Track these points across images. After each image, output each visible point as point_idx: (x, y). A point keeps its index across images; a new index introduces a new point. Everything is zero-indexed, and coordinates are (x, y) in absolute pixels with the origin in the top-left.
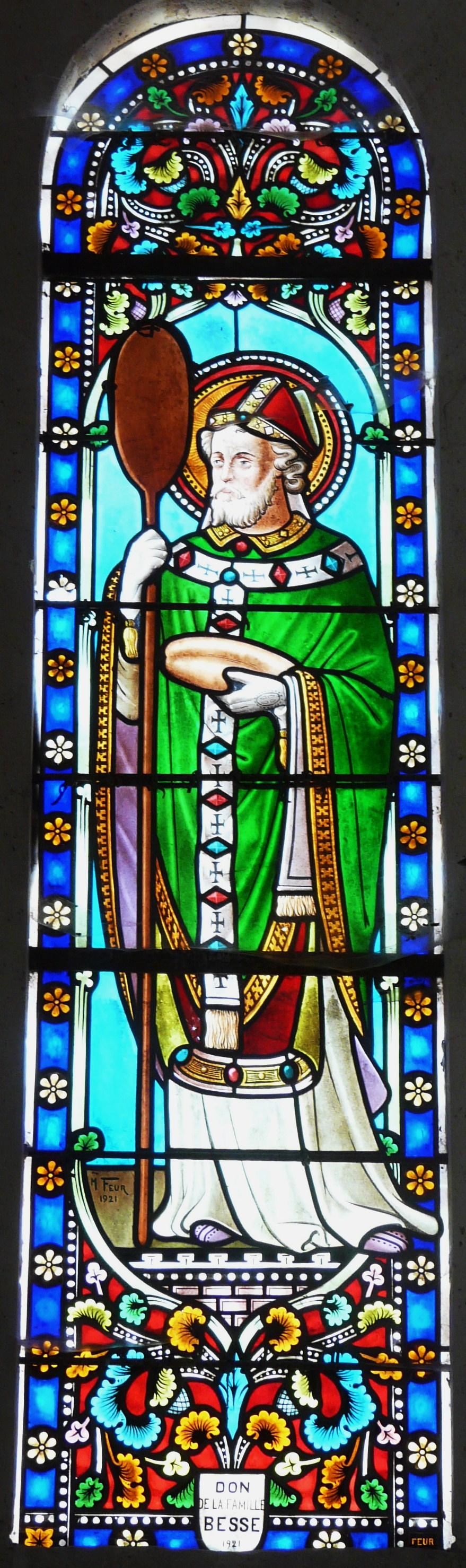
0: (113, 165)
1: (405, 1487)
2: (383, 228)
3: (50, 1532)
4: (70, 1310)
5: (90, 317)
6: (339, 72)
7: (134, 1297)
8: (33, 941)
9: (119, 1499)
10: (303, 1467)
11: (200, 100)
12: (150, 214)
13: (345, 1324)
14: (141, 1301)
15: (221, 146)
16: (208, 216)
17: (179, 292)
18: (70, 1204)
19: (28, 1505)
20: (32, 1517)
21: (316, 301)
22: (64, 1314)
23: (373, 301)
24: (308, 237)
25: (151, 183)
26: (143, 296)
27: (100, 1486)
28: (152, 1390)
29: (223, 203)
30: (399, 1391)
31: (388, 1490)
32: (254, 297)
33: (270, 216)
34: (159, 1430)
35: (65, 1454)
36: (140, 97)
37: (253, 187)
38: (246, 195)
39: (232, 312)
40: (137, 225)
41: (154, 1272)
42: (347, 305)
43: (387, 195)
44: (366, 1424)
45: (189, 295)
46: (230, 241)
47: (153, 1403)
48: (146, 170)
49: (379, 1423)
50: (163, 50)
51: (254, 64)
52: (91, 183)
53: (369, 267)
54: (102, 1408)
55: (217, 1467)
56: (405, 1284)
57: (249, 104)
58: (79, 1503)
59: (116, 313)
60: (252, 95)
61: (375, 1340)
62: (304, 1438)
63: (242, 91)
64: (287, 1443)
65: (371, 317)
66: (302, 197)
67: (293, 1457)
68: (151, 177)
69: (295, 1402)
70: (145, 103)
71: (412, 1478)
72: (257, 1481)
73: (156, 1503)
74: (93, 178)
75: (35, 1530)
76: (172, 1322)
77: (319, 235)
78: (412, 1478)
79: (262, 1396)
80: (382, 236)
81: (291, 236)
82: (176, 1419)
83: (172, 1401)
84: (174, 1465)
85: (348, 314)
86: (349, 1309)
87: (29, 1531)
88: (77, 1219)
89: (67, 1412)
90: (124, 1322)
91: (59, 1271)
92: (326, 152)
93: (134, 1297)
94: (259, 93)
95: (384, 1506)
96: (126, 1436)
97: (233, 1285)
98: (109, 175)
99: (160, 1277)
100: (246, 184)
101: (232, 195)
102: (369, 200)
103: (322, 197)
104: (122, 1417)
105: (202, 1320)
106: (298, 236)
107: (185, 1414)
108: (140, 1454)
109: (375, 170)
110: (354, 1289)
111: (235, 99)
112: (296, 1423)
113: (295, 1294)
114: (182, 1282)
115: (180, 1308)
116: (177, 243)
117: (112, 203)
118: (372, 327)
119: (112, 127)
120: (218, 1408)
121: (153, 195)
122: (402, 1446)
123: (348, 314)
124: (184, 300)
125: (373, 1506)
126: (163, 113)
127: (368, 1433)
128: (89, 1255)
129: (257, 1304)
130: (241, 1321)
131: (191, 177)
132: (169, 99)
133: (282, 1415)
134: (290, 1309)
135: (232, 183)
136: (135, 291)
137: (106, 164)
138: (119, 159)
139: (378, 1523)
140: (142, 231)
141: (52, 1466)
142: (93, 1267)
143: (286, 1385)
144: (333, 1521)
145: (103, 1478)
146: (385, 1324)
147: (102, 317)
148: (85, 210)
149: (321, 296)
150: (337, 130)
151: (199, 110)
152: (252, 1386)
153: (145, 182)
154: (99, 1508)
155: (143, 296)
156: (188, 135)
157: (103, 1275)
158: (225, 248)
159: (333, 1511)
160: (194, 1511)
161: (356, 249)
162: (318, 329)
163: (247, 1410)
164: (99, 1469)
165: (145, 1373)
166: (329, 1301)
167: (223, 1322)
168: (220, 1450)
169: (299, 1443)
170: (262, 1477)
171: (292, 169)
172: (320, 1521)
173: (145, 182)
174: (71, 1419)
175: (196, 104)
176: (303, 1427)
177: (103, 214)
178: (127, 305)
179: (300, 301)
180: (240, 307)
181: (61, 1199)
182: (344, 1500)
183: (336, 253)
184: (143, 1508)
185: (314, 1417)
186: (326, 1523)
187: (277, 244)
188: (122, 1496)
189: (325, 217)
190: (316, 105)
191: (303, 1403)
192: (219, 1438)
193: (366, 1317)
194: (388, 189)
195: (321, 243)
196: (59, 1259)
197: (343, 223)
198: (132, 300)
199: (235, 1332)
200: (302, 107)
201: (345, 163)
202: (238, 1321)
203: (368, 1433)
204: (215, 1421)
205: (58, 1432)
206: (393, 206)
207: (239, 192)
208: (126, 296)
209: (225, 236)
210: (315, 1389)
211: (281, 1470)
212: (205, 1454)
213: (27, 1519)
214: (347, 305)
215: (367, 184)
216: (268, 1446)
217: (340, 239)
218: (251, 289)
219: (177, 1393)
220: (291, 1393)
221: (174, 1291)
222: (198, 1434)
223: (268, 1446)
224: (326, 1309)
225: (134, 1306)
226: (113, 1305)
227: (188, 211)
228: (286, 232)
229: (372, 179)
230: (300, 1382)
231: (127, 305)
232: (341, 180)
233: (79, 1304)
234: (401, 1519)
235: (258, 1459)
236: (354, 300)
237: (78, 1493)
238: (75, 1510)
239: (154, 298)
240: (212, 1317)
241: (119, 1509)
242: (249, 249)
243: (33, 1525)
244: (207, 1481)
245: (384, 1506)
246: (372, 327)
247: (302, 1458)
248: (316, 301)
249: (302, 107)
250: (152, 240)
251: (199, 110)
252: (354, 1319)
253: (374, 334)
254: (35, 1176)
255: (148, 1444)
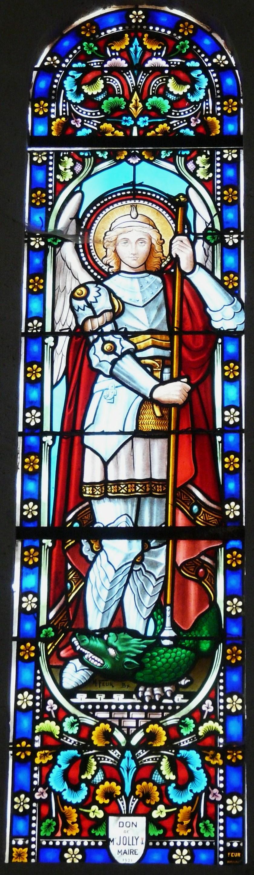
0: (65, 86)
1: (224, 824)
2: (218, 118)
3: (26, 850)
4: (37, 727)
5: (51, 172)
6: (191, 32)
7: (72, 718)
8: (18, 523)
9: (65, 830)
10: (166, 813)
11: (113, 48)
12: (85, 112)
13: (191, 734)
14: (76, 720)
15: (124, 74)
16: (118, 114)
17: (100, 155)
18: (38, 666)
19: (14, 833)
20: (16, 842)
21: (180, 161)
22: (34, 729)
23: (211, 160)
24: (175, 125)
25: (86, 95)
26: (81, 160)
27: (54, 823)
28: (84, 769)
29: (127, 106)
30: (221, 771)
31: (215, 827)
32: (146, 157)
33: (153, 114)
34: (86, 793)
35: (34, 805)
36: (79, 48)
37: (144, 98)
38: (139, 102)
39: (132, 167)
40: (80, 120)
41: (86, 704)
42: (197, 162)
43: (218, 100)
44: (203, 788)
45: (106, 157)
46: (131, 127)
47: (83, 777)
48: (84, 87)
49: (210, 788)
50: (91, 21)
51: (142, 27)
52: (53, 97)
53: (204, 140)
54: (56, 781)
55: (119, 812)
56: (225, 710)
57: (140, 49)
58: (42, 834)
59: (65, 169)
60: (141, 44)
61: (209, 741)
62: (168, 795)
63: (136, 42)
64: (158, 799)
65: (211, 170)
66: (171, 103)
67: (161, 807)
68: (86, 91)
69: (163, 777)
70: (83, 52)
71: (228, 819)
72: (141, 821)
73: (85, 834)
74: (54, 95)
75: (18, 849)
76: (94, 733)
77: (180, 124)
78: (228, 819)
79: (144, 773)
80: (218, 122)
81: (165, 125)
82: (97, 786)
83: (93, 776)
84: (96, 813)
85: (198, 167)
86: (194, 726)
87: (14, 849)
88: (41, 675)
89: (35, 783)
90: (67, 733)
91: (30, 704)
92: (182, 75)
93: (72, 718)
94: (145, 43)
95: (213, 835)
96: (67, 796)
97: (129, 712)
98: (63, 91)
99: (82, 707)
100: (140, 95)
101: (132, 102)
102: (208, 102)
103: (179, 103)
104: (66, 786)
105: (110, 730)
106: (169, 125)
107: (103, 782)
108: (76, 806)
109: (210, 85)
110: (62, 714)
111: (132, 46)
112: (163, 788)
113: (163, 718)
114: (102, 710)
115: (98, 725)
116: (101, 129)
117: (65, 108)
118: (211, 175)
119: (64, 65)
120: (120, 781)
121: (90, 102)
122: (223, 802)
123: (198, 167)
124: (103, 160)
125: (206, 835)
126: (93, 56)
127: (204, 794)
128: (47, 695)
129: (142, 723)
130: (133, 731)
131: (109, 90)
132: (96, 48)
133: (155, 783)
134: (160, 725)
135: (132, 95)
136: (76, 157)
137: (61, 86)
138: (68, 83)
139: (208, 844)
140: (82, 123)
141: (27, 814)
142: (50, 702)
143: (157, 766)
144: (182, 843)
145: (56, 819)
146: (213, 734)
147: (58, 171)
148: (49, 113)
149: (183, 158)
150: (188, 64)
151: (114, 54)
152: (139, 767)
153: (82, 95)
154: (53, 836)
155: (81, 160)
156: (107, 69)
157: (55, 707)
158: (128, 133)
159: (183, 837)
160: (107, 840)
161: (201, 130)
162: (180, 175)
163: (136, 781)
164: (54, 815)
165: (81, 764)
166: (183, 721)
167: (122, 732)
168: (120, 803)
169: (165, 800)
170: (144, 819)
171: (165, 87)
172: (175, 843)
173: (82, 95)
174: (37, 787)
175: (112, 51)
176: (167, 790)
177: (61, 114)
178: (72, 164)
179: (171, 160)
180: (137, 164)
181: (32, 665)
182: (189, 831)
183: (192, 133)
184: (78, 836)
185: (173, 785)
186: (72, 844)
187: (157, 130)
188: (67, 828)
189: (185, 113)
190: (178, 49)
191: (167, 778)
192: (119, 797)
193: (202, 731)
194: (219, 96)
195: (184, 128)
196: (31, 697)
197: (195, 115)
198: (75, 161)
199: (129, 737)
200: (169, 51)
201: (194, 81)
202: (132, 730)
203: (204, 794)
204: (119, 788)
205: (30, 794)
206: (222, 106)
207: (136, 101)
208: (71, 160)
209: (128, 125)
210: (173, 768)
211: (155, 814)
212: (112, 809)
213: (14, 842)
214: (197, 162)
215: (206, 92)
216: (148, 802)
217: (193, 125)
218: (143, 153)
219: (96, 772)
220: (160, 772)
221: (96, 715)
222: (108, 794)
223: (148, 802)
224: (180, 726)
225: (72, 725)
226: (59, 723)
227: (108, 110)
228: (162, 123)
229: (209, 91)
230: (165, 763)
231: (72, 164)
232: (192, 91)
233: (41, 724)
234: (222, 842)
235: (142, 809)
236: (201, 160)
237: (42, 828)
238: (40, 837)
239: (86, 159)
240: (116, 729)
241: (64, 836)
242: (142, 132)
243: (17, 846)
244: (112, 819)
245: (213, 835)
246: (211, 175)
247: (166, 808)
248: (180, 161)
249: (169, 51)
250: (87, 128)
251: (114, 54)
252: (196, 730)
253: (212, 179)
254: (19, 650)
255: (80, 801)
